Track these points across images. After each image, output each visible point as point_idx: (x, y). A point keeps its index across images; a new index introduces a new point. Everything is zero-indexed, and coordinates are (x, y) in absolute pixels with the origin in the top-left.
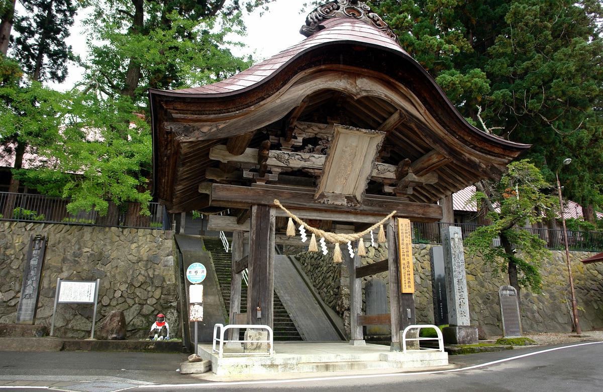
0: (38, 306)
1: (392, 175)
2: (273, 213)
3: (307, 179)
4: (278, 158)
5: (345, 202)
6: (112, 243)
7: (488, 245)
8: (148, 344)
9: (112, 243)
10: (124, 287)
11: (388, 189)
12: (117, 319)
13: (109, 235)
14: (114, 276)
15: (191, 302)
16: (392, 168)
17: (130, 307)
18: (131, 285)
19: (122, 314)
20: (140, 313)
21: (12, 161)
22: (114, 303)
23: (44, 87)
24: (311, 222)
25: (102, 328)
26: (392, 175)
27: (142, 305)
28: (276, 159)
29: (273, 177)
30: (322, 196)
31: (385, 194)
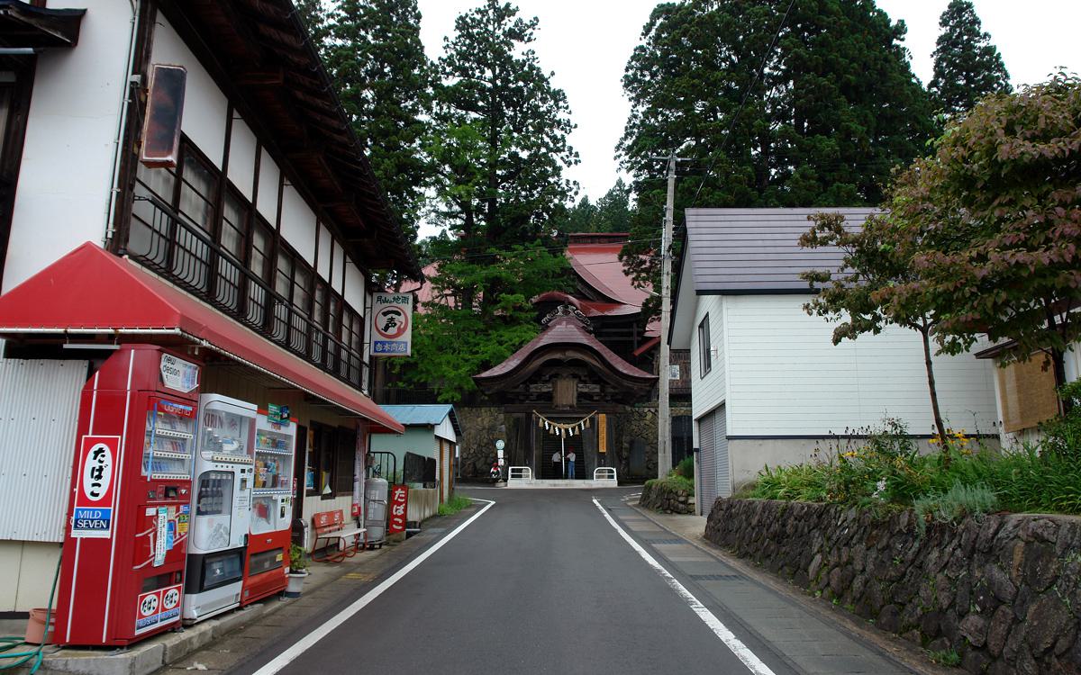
0: (205, 584)
1: (598, 390)
2: (533, 415)
3: (549, 397)
4: (536, 388)
5: (568, 408)
6: (466, 418)
7: (488, 461)
8: (488, 479)
9: (466, 418)
10: (475, 447)
11: (595, 398)
12: (471, 466)
13: (463, 413)
14: (469, 440)
15: (47, 607)
16: (598, 386)
17: (480, 458)
18: (479, 445)
19: (474, 464)
20: (485, 463)
21: (312, 506)
22: (470, 456)
23: (364, 95)
24: (547, 418)
25: (464, 471)
26: (598, 390)
27: (487, 457)
28: (534, 388)
29: (534, 397)
30: (557, 406)
31: (593, 401)
